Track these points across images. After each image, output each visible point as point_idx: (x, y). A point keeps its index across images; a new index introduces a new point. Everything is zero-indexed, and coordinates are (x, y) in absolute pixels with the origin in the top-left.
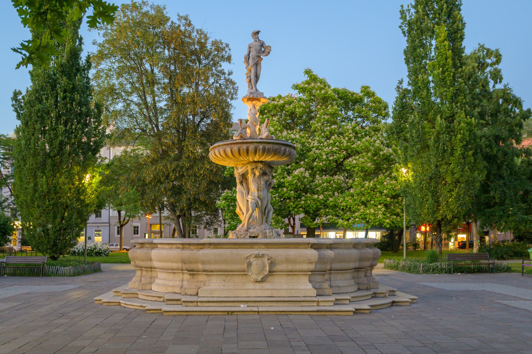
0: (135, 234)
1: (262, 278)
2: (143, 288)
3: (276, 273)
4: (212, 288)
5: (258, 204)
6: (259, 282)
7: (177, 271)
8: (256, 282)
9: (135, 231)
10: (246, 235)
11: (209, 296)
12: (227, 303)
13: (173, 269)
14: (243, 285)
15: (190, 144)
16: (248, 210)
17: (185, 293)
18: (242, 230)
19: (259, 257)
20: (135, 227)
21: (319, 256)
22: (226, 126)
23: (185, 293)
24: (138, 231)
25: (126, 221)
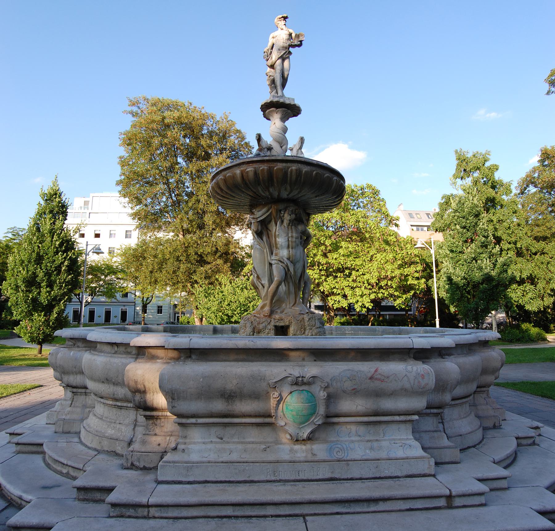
0: (158, 313)
1: (312, 432)
2: (66, 429)
3: (342, 419)
4: (195, 457)
5: (289, 270)
6: (303, 440)
7: (125, 404)
8: (297, 440)
9: (158, 310)
10: (269, 324)
11: (184, 479)
12: (222, 508)
13: (116, 400)
14: (265, 450)
15: (238, 287)
16: (271, 281)
17: (132, 464)
18: (262, 316)
19: (304, 384)
20: (159, 307)
21: (436, 378)
22: (239, 139)
23: (132, 464)
24: (161, 310)
25: (148, 302)
